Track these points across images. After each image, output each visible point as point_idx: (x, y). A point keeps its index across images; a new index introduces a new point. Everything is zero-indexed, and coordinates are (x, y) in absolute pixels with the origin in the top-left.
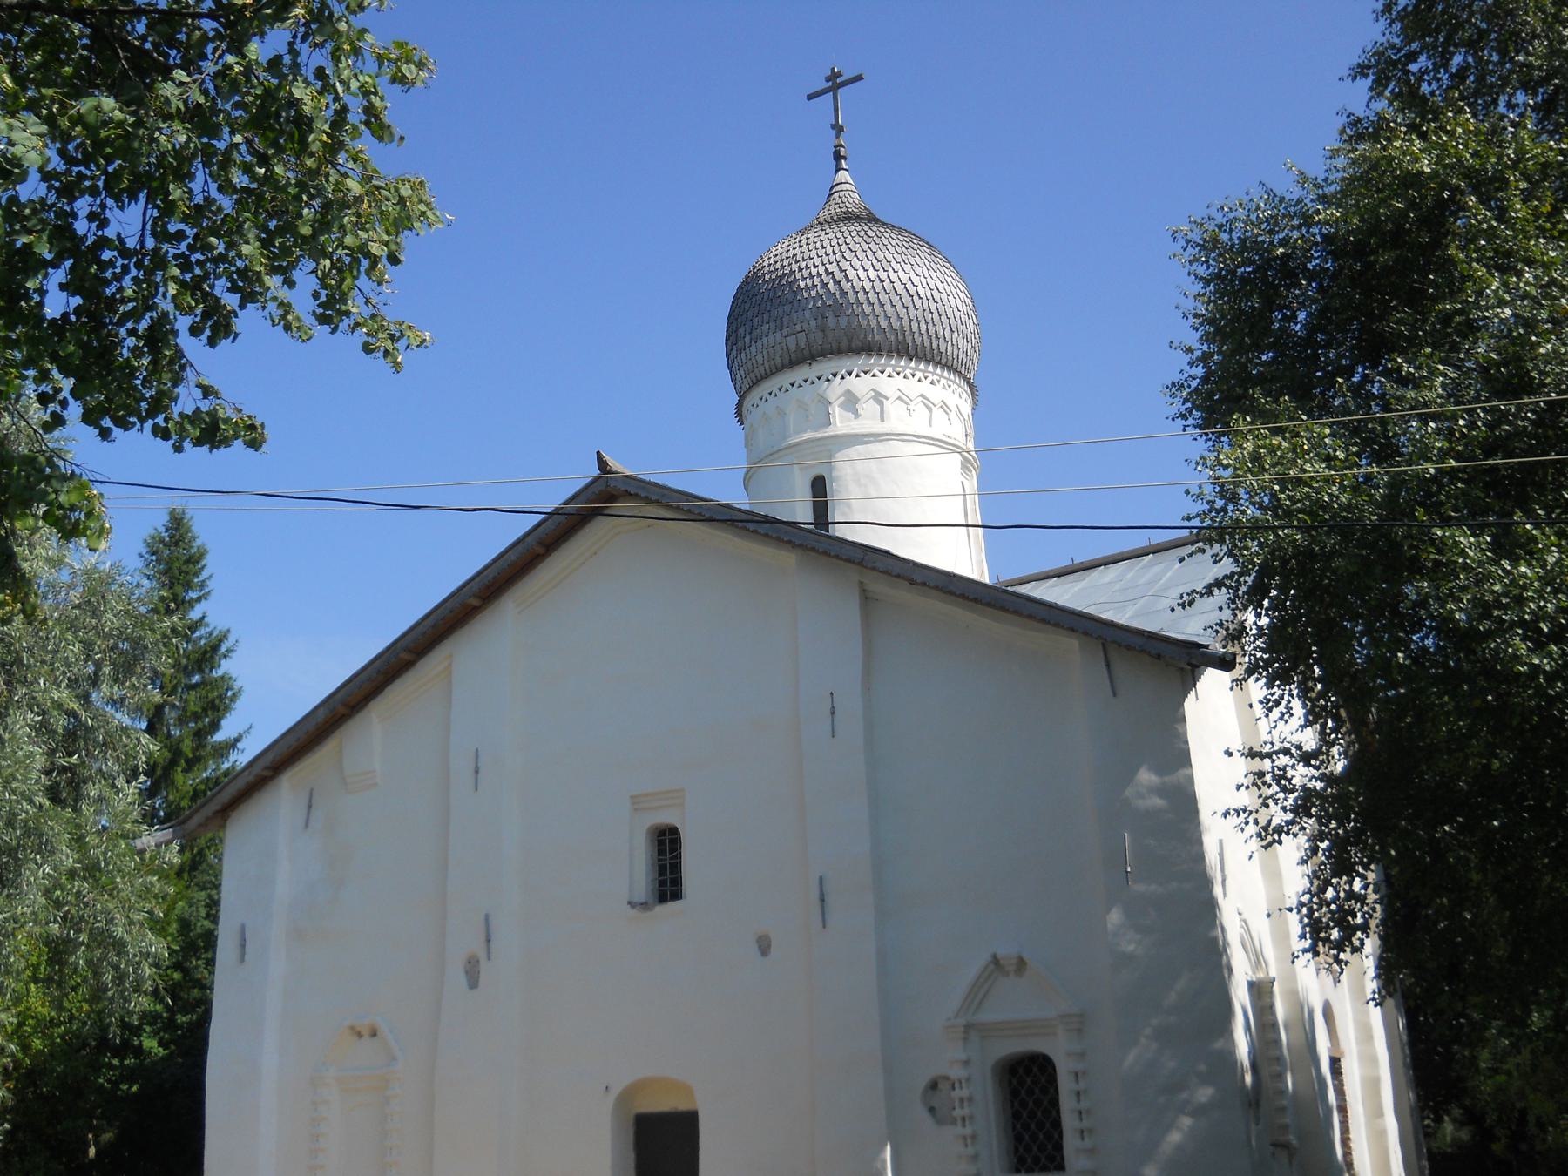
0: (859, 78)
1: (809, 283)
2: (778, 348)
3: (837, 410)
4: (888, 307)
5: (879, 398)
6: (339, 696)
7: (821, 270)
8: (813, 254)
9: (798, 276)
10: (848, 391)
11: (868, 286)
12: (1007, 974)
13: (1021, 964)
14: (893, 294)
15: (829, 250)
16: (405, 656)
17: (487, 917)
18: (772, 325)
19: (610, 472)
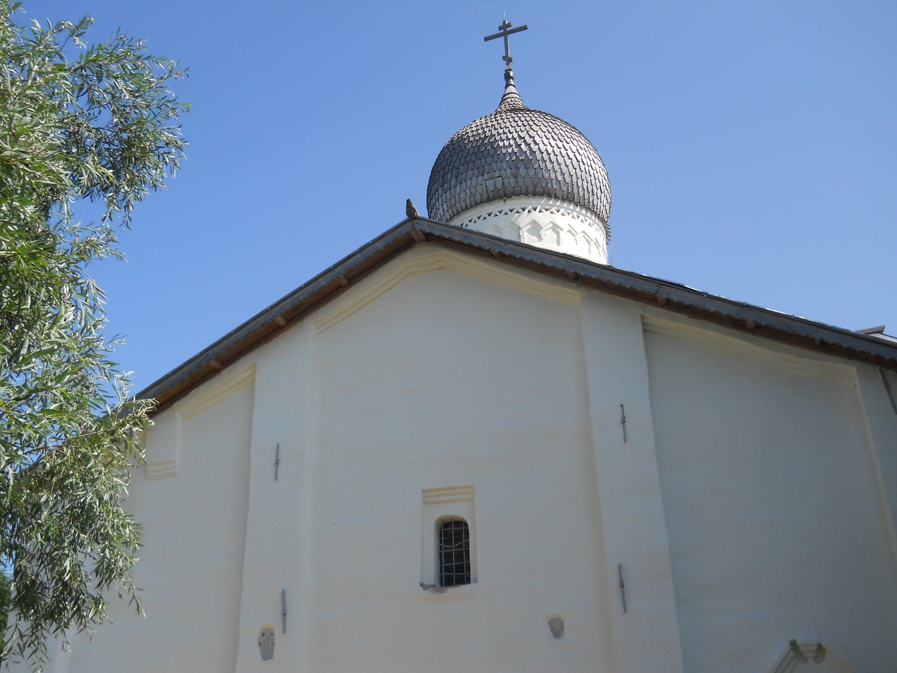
0: (524, 28)
1: (506, 143)
2: (479, 188)
3: (526, 233)
4: (563, 166)
5: (556, 228)
6: (261, 319)
7: (516, 135)
8: (508, 124)
9: (498, 138)
10: (534, 222)
11: (550, 150)
12: (805, 660)
13: (820, 648)
14: (566, 158)
15: (520, 123)
16: (213, 363)
17: (283, 592)
18: (476, 171)
19: (417, 218)
